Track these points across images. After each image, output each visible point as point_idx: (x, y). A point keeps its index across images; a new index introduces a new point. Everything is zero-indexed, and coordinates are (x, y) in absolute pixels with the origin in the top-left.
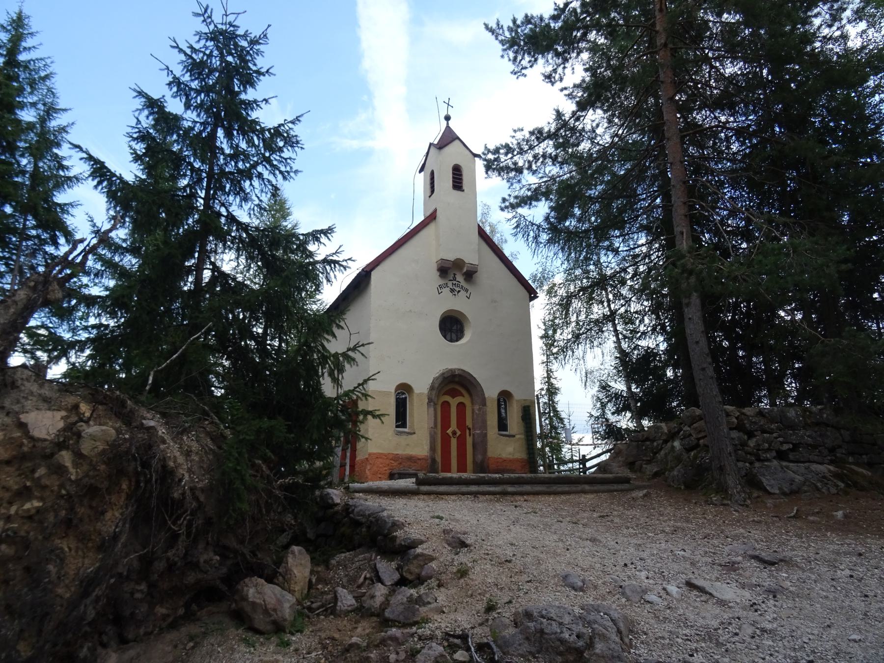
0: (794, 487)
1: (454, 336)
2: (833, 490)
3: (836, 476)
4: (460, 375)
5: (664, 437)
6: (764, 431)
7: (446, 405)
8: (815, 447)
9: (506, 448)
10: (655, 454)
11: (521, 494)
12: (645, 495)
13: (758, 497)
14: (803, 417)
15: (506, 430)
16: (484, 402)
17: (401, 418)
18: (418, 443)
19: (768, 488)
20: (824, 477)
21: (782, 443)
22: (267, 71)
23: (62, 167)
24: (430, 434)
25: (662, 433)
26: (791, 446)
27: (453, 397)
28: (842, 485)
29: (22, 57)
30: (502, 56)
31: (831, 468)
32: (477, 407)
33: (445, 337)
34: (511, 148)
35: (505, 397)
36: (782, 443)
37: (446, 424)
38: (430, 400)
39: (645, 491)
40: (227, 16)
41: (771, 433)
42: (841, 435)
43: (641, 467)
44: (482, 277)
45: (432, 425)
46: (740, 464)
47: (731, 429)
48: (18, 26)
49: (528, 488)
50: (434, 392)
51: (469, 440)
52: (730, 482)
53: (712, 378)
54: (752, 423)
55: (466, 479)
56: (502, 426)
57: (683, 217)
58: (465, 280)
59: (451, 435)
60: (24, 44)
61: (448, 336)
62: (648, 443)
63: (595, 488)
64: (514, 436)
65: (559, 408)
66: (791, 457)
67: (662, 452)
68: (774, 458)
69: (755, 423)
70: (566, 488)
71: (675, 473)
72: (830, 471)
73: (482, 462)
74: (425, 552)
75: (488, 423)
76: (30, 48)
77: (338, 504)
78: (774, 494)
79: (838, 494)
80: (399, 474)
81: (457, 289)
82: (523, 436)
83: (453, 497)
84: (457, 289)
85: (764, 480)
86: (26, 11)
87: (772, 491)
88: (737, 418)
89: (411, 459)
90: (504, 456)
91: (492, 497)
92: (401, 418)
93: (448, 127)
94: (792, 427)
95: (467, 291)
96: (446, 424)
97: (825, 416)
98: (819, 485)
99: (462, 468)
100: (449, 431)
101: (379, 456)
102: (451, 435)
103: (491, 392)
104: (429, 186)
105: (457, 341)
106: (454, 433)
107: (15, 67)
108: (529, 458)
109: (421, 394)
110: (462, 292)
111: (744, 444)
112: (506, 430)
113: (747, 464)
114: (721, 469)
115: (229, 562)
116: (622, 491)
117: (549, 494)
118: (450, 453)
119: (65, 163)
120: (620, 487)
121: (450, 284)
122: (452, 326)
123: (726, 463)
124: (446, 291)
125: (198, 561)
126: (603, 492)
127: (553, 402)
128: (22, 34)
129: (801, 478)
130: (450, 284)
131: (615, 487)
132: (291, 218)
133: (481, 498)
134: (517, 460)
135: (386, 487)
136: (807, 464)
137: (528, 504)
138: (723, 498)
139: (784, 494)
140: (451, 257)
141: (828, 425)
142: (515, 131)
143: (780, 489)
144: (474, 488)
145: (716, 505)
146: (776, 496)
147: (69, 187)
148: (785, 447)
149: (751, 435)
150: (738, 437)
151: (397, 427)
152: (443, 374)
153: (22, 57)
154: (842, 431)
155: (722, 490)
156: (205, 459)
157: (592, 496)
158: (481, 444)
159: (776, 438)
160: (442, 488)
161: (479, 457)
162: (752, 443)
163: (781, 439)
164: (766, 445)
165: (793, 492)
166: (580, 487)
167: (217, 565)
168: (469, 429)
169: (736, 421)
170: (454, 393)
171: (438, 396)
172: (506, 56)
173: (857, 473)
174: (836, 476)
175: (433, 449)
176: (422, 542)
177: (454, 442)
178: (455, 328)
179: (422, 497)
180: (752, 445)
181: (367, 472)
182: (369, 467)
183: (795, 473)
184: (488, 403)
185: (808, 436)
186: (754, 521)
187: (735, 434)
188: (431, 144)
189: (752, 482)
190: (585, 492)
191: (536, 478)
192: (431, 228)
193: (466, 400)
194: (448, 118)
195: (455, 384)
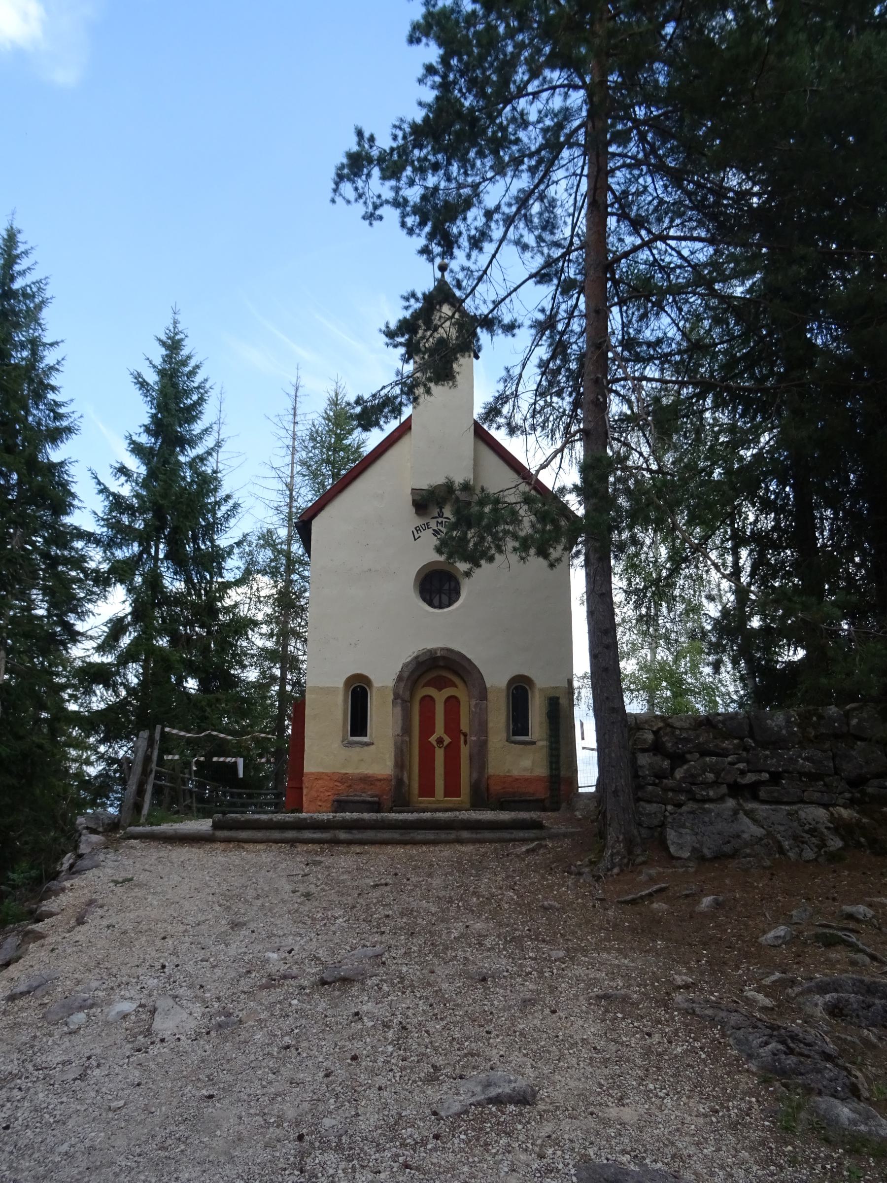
1: (445, 599)
4: (443, 658)
6: (704, 753)
7: (428, 701)
8: (813, 777)
16: (483, 693)
17: (358, 723)
18: (377, 758)
19: (672, 849)
21: (743, 773)
23: (58, 417)
24: (395, 743)
26: (765, 776)
27: (440, 689)
28: (835, 843)
29: (17, 285)
32: (473, 702)
33: (431, 604)
35: (519, 689)
36: (743, 773)
38: (396, 696)
41: (724, 754)
49: (369, 835)
50: (402, 685)
59: (435, 744)
60: (17, 268)
61: (436, 601)
63: (479, 836)
64: (533, 743)
66: (762, 794)
69: (687, 740)
70: (430, 835)
75: (490, 725)
76: (24, 271)
78: (679, 858)
79: (816, 860)
88: (655, 733)
89: (366, 780)
90: (515, 773)
92: (358, 723)
94: (776, 743)
98: (786, 844)
99: (452, 789)
100: (433, 739)
101: (319, 777)
102: (435, 744)
103: (496, 679)
105: (449, 605)
106: (440, 741)
108: (551, 776)
109: (382, 689)
116: (514, 840)
117: (404, 843)
118: (433, 769)
119: (62, 410)
121: (433, 524)
126: (491, 841)
129: (758, 831)
130: (433, 524)
134: (539, 779)
136: (795, 807)
143: (694, 850)
144: (290, 834)
147: (62, 442)
148: (750, 778)
149: (678, 759)
152: (417, 657)
159: (732, 764)
160: (243, 835)
163: (741, 766)
164: (710, 776)
166: (453, 835)
168: (465, 735)
170: (440, 683)
172: (339, 199)
175: (401, 763)
177: (440, 754)
178: (446, 587)
184: (490, 696)
185: (806, 759)
187: (644, 760)
190: (461, 842)
193: (460, 692)
195: (438, 671)
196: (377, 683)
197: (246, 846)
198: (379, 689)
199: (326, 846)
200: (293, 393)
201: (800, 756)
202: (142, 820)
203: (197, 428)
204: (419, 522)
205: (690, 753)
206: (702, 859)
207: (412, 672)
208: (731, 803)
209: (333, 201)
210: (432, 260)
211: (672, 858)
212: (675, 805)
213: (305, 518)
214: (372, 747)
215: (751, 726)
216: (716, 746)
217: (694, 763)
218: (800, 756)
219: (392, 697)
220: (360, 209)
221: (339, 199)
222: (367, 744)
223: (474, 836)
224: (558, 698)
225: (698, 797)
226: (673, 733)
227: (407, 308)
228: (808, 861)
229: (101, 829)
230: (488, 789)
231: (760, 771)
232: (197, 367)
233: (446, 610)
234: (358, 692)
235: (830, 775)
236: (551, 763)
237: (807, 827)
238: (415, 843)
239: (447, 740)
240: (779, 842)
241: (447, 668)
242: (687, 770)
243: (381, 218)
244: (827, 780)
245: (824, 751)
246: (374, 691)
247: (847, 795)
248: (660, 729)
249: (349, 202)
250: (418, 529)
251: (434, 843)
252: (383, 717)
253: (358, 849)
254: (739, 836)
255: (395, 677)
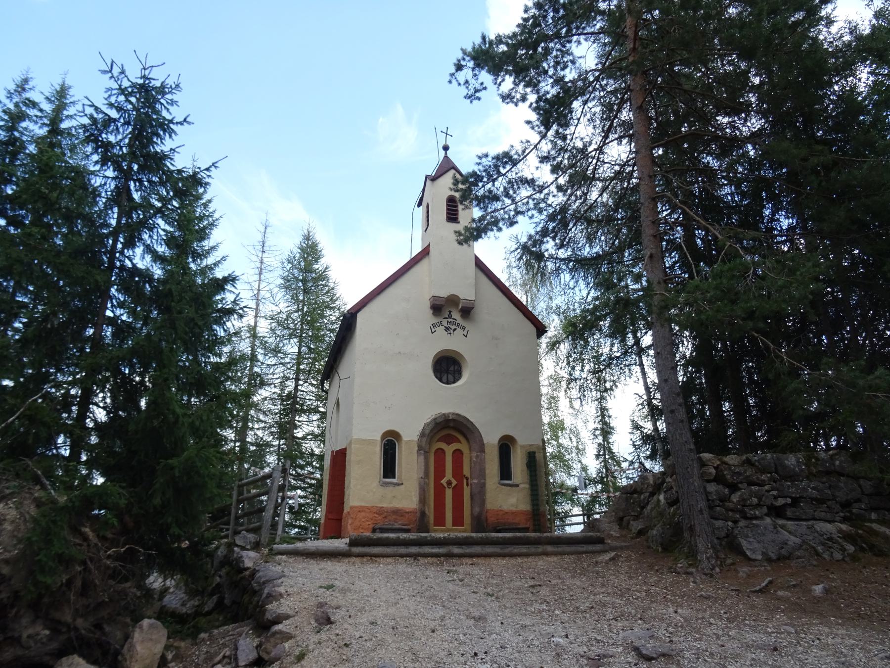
0: (783, 552)
1: (451, 377)
2: (838, 556)
3: (847, 537)
4: (454, 420)
5: (650, 490)
6: (751, 484)
7: (440, 453)
8: (821, 501)
9: (508, 500)
10: (643, 508)
11: (471, 556)
12: (612, 559)
13: (733, 564)
14: (806, 465)
15: (510, 479)
16: (482, 448)
17: (389, 469)
18: (406, 495)
19: (748, 553)
20: (830, 539)
21: (776, 498)
22: (185, 120)
24: (420, 484)
25: (648, 484)
26: (789, 500)
28: (851, 548)
29: (64, 125)
30: (450, 82)
31: (844, 527)
32: (474, 454)
33: (441, 380)
34: (478, 176)
35: (506, 445)
36: (776, 498)
37: (440, 472)
38: (420, 448)
39: (613, 554)
40: (145, 69)
41: (761, 484)
42: (860, 486)
43: (629, 523)
44: (483, 313)
45: (422, 475)
46: (719, 523)
47: (709, 481)
48: (61, 97)
50: (425, 439)
51: (467, 491)
52: (700, 545)
53: (682, 421)
54: (735, 474)
55: (405, 539)
56: (505, 473)
57: (652, 238)
58: (462, 316)
59: (445, 485)
60: (65, 113)
61: (444, 379)
62: (635, 496)
64: (517, 486)
65: (615, 449)
66: (789, 513)
67: (649, 507)
68: (767, 515)
69: (739, 474)
70: (524, 549)
71: (655, 532)
72: (840, 531)
73: (480, 514)
74: (284, 629)
75: (487, 472)
77: (248, 568)
78: (755, 560)
79: (843, 560)
80: (380, 529)
81: (453, 327)
82: (527, 486)
83: (389, 560)
84: (453, 327)
85: (744, 543)
86: (68, 82)
87: (753, 557)
88: (716, 468)
89: (397, 512)
91: (435, 560)
92: (389, 469)
93: (446, 157)
94: (792, 477)
95: (464, 328)
96: (440, 472)
97: (837, 463)
98: (820, 549)
99: (458, 521)
100: (444, 482)
101: (361, 509)
102: (445, 485)
103: (491, 438)
104: (425, 220)
105: (454, 382)
106: (449, 483)
107: (58, 134)
108: (534, 510)
110: (459, 330)
111: (724, 499)
112: (510, 479)
113: (730, 523)
114: (691, 529)
115: (63, 638)
116: (593, 552)
117: (504, 556)
120: (591, 548)
121: (445, 323)
122: (447, 367)
123: (696, 522)
124: (440, 330)
125: (20, 636)
126: (569, 554)
127: (608, 443)
128: (66, 104)
129: (798, 541)
130: (445, 323)
131: (585, 548)
132: (322, 261)
133: (422, 560)
134: (522, 513)
135: (314, 549)
136: (810, 523)
137: (477, 571)
138: (690, 565)
139: (769, 560)
140: (444, 293)
141: (841, 474)
142: (480, 158)
143: (763, 554)
144: (413, 550)
145: (679, 573)
146: (757, 563)
148: (781, 502)
149: (734, 488)
150: (716, 491)
151: (384, 477)
152: (435, 419)
153: (64, 125)
154: (862, 482)
155: (692, 555)
156: (22, 527)
157: (555, 559)
158: (479, 495)
159: (768, 491)
161: (477, 510)
162: (735, 498)
163: (775, 493)
164: (755, 500)
165: (780, 558)
166: (540, 549)
167: (45, 640)
168: (467, 479)
169: (713, 471)
170: (449, 440)
171: (430, 443)
172: (454, 81)
173: (876, 533)
174: (847, 537)
175: (423, 500)
176: (287, 617)
177: (449, 493)
178: (452, 368)
179: (353, 559)
180: (735, 501)
181: (349, 527)
182: (350, 522)
183: (791, 533)
185: (813, 488)
186: (701, 596)
187: (712, 488)
188: (427, 177)
189: (731, 545)
190: (547, 554)
191: (487, 538)
192: (424, 263)
193: (463, 446)
194: (446, 148)
195: (450, 429)
196: (405, 438)
197: (378, 559)
198: (407, 442)
199: (442, 559)
200: (263, 230)
201: (809, 486)
202: (278, 540)
203: (207, 244)
204: (435, 320)
205: (741, 483)
206: (769, 560)
207: (431, 431)
208: (768, 520)
209: (450, 82)
210: (533, 128)
211: (750, 559)
212: (733, 522)
213: (353, 311)
214: (402, 487)
215: (775, 465)
216: (758, 478)
217: (744, 490)
218: (809, 486)
219: (416, 448)
220: (463, 91)
221: (454, 81)
222: (398, 485)
223: (556, 549)
224: (534, 453)
225: (748, 515)
226: (730, 469)
227: (479, 164)
228: (838, 561)
229: (248, 547)
230: (487, 520)
231: (786, 497)
232: (210, 201)
233: (453, 385)
234: (390, 444)
235: (829, 500)
236: (532, 500)
237: (825, 537)
238: (512, 555)
239: (454, 483)
240: (813, 547)
241: (448, 427)
242: (741, 495)
243: (479, 99)
244: (829, 503)
245: (823, 483)
246: (403, 445)
247: (842, 514)
248: (718, 465)
249: (459, 84)
250: (434, 325)
251: (527, 555)
252: (409, 463)
253: (469, 561)
254: (786, 544)
255: (419, 433)
